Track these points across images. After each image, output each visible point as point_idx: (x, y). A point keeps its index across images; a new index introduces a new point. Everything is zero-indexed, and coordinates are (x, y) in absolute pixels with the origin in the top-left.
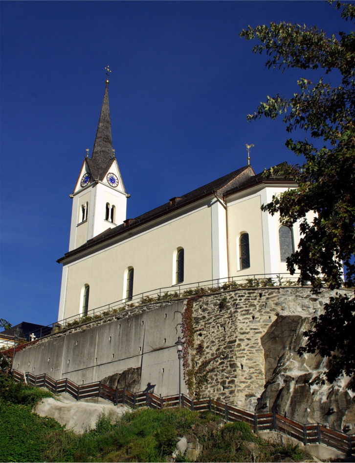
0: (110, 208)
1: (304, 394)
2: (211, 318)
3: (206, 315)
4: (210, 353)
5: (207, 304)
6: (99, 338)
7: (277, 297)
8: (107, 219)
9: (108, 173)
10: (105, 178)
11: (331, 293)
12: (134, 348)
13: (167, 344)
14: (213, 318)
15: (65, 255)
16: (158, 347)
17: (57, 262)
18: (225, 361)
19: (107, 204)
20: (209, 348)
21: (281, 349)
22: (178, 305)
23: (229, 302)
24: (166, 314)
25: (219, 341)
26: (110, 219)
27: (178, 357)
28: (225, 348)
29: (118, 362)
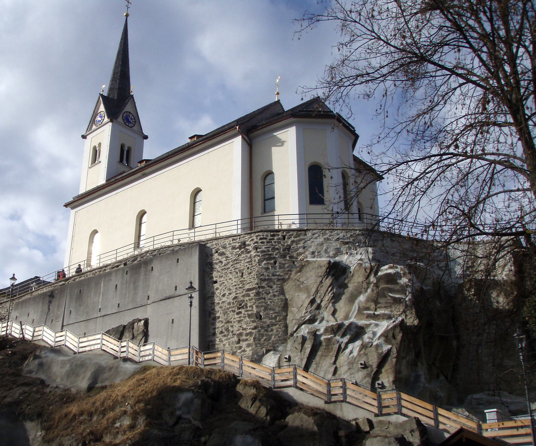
0: (126, 149)
1: (330, 347)
2: (228, 263)
3: (223, 260)
4: (227, 303)
5: (224, 247)
6: (104, 286)
7: (303, 241)
8: (121, 160)
9: (124, 111)
10: (121, 116)
11: (262, 412)
12: (140, 298)
13: (178, 292)
14: (231, 263)
15: (73, 198)
16: (168, 295)
17: (64, 206)
18: (243, 311)
19: (122, 147)
20: (225, 297)
21: (306, 298)
22: (173, 254)
23: (249, 245)
24: (127, 271)
25: (236, 288)
26: (125, 162)
27: (193, 304)
28: (243, 296)
29: (133, 310)
